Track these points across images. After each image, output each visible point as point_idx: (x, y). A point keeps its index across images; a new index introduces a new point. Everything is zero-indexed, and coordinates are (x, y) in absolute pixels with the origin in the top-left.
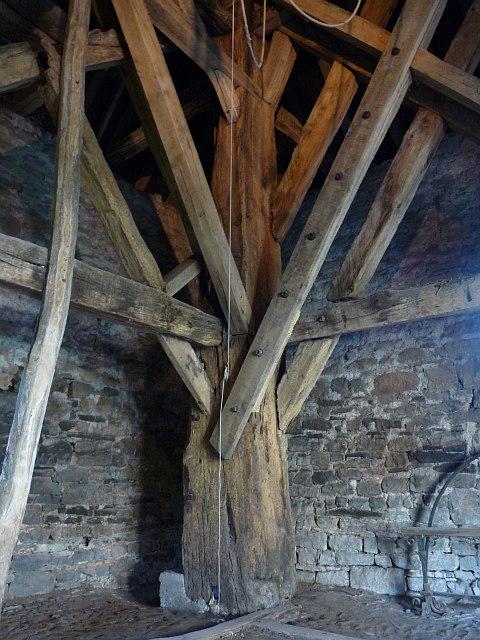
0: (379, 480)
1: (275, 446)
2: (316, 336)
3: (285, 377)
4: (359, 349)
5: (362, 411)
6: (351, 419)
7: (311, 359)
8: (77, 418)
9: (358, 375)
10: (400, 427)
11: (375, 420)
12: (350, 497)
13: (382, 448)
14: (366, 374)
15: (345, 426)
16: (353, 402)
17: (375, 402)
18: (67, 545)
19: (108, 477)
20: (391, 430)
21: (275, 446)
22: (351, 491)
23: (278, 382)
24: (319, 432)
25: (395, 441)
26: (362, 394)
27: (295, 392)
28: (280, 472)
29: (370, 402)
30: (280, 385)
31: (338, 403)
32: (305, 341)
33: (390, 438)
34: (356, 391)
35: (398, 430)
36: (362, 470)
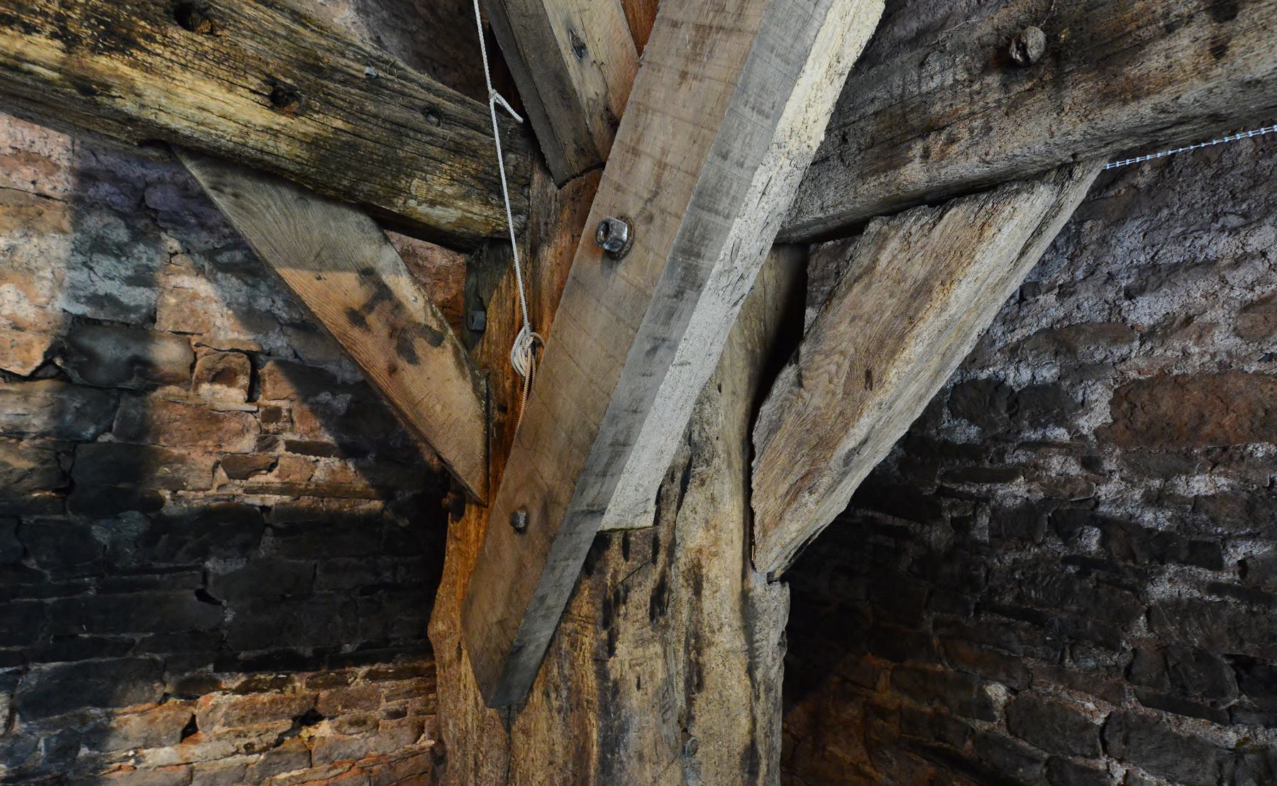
0: (1095, 711)
1: (727, 639)
2: (965, 167)
3: (789, 373)
4: (1061, 296)
5: (1053, 488)
6: (1009, 503)
7: (923, 291)
8: (281, 449)
9: (1048, 374)
10: (1217, 565)
11: (1105, 524)
12: (981, 726)
13: (1125, 618)
14: (1083, 372)
15: (984, 520)
16: (1021, 456)
17: (1109, 465)
18: (241, 742)
19: (370, 579)
20: (1172, 568)
21: (727, 639)
22: (985, 708)
23: (761, 390)
24: (899, 522)
25: (1176, 607)
26: (1061, 434)
27: (826, 444)
28: (744, 722)
29: (1090, 463)
30: (766, 409)
31: (968, 450)
32: (897, 207)
33: (1161, 590)
34: (1034, 425)
35: (1207, 575)
36: (1030, 663)
